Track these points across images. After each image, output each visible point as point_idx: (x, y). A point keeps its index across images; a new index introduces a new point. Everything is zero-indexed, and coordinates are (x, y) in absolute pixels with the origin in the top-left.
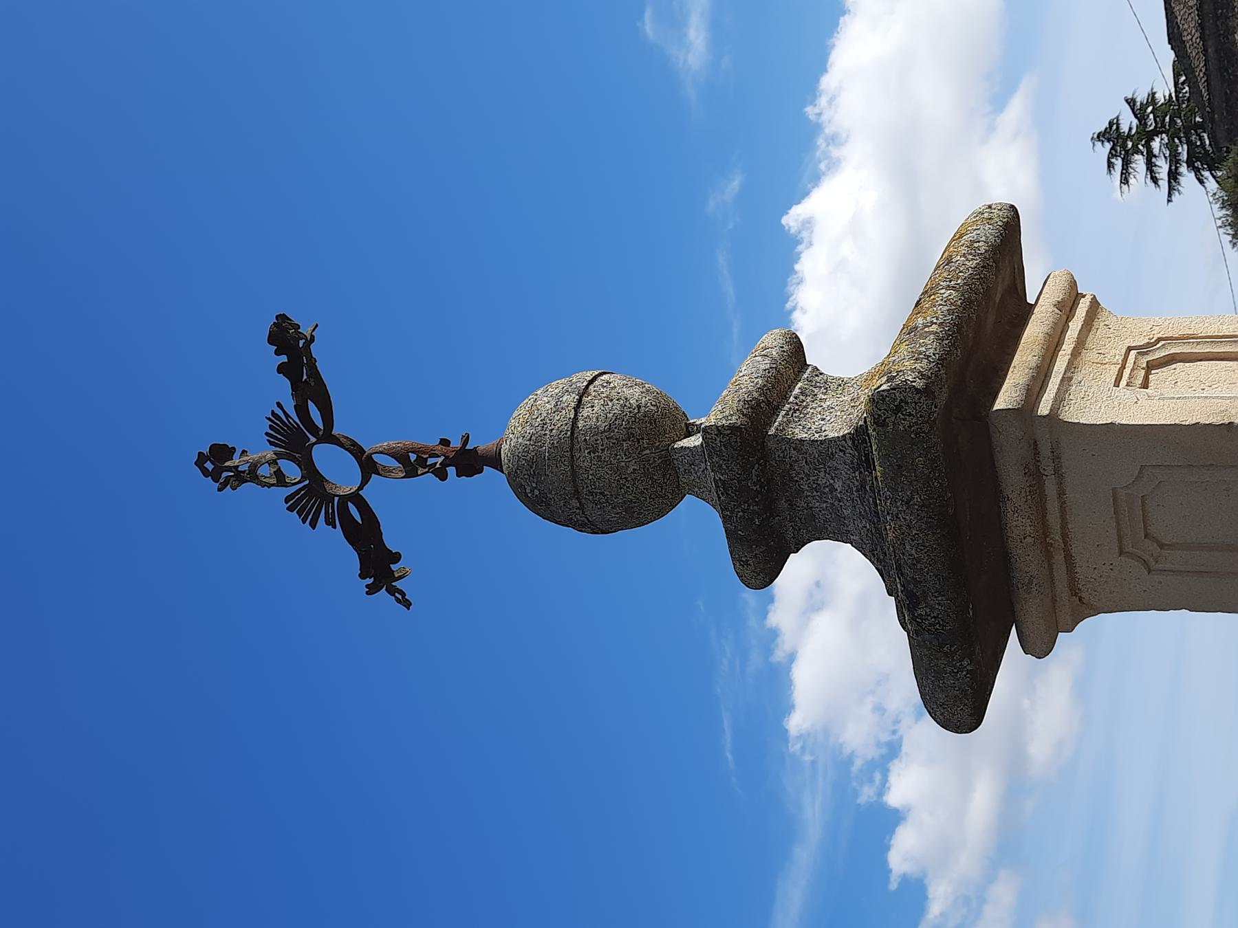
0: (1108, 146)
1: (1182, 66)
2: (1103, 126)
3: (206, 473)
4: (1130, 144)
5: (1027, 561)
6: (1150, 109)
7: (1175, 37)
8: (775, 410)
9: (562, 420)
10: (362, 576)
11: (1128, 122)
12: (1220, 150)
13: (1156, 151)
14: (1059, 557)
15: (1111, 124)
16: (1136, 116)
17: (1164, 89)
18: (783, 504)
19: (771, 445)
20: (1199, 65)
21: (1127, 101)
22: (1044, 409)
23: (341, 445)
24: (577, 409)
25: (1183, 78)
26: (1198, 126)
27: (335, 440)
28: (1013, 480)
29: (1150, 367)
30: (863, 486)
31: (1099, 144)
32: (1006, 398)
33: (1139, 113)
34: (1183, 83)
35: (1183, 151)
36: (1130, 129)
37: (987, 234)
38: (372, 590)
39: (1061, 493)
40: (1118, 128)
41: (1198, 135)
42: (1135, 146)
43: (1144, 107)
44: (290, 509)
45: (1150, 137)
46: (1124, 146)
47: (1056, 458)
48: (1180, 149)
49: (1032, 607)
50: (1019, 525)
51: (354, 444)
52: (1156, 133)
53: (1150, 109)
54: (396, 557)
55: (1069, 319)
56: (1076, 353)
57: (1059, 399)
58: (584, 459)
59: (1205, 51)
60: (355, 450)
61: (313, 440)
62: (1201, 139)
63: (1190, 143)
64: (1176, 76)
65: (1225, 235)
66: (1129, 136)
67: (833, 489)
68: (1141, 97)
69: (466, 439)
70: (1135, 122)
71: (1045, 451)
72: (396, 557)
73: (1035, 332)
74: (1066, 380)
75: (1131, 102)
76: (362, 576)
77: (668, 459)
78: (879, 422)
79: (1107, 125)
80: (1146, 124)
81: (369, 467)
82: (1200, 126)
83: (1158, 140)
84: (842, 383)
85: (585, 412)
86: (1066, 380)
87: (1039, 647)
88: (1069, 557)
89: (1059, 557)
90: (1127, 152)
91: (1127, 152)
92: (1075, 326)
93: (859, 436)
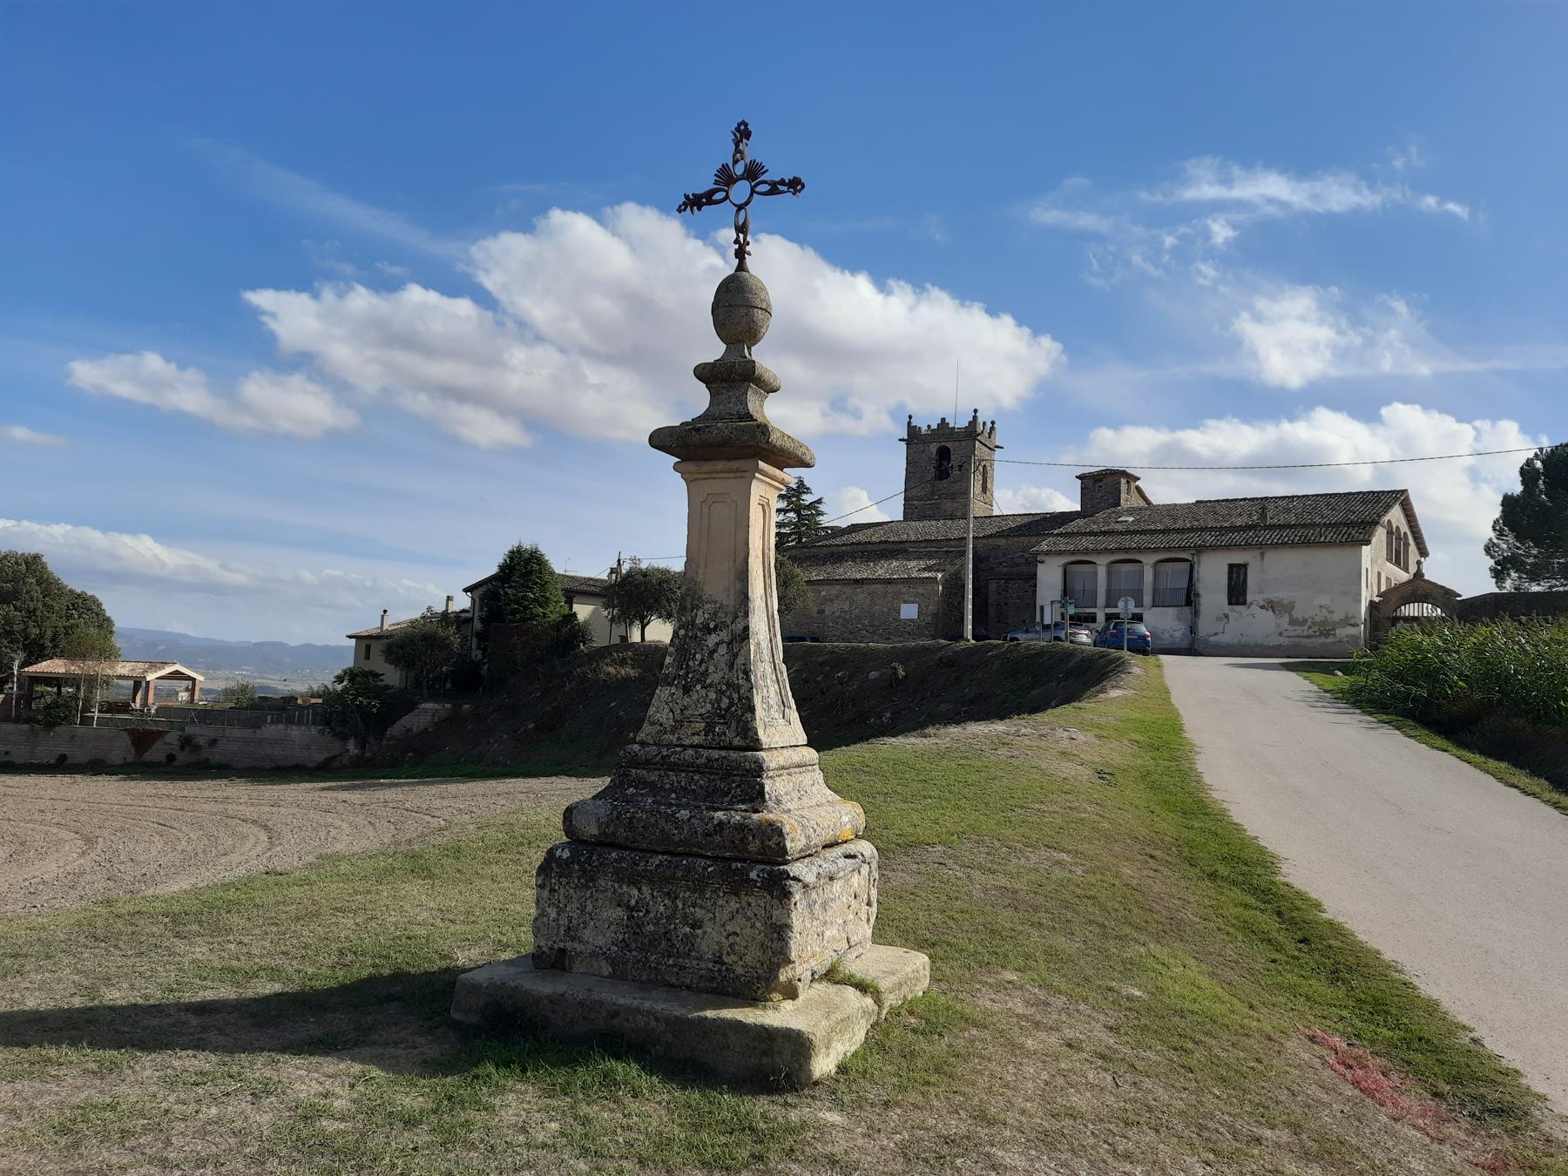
0: (795, 486)
1: (837, 532)
2: (807, 484)
3: (739, 125)
4: (794, 499)
5: (707, 466)
6: (814, 512)
7: (855, 528)
8: (757, 385)
9: (758, 303)
10: (693, 195)
11: (808, 499)
12: (784, 551)
13: (788, 515)
14: (708, 476)
15: (808, 489)
16: (811, 504)
17: (825, 521)
18: (724, 385)
19: (747, 383)
20: (838, 541)
21: (821, 499)
22: (757, 475)
23: (749, 197)
24: (761, 308)
25: (830, 532)
26: (800, 540)
27: (751, 195)
28: (735, 464)
29: (763, 505)
30: (731, 415)
31: (796, 481)
32: (762, 464)
33: (812, 506)
34: (827, 532)
35: (786, 530)
36: (803, 500)
37: (807, 459)
38: (687, 197)
39: (729, 478)
40: (805, 493)
41: (794, 540)
42: (792, 502)
43: (815, 508)
44: (723, 165)
45: (797, 512)
46: (793, 496)
47: (741, 477)
48: (787, 529)
49: (690, 466)
50: (720, 465)
51: (749, 203)
52: (799, 515)
53: (814, 512)
54: (699, 209)
55: (779, 483)
56: (769, 484)
57: (759, 479)
58: (743, 311)
59: (844, 545)
60: (747, 203)
61: (753, 184)
62: (792, 541)
63: (790, 534)
64: (832, 528)
65: (1001, 445)
66: (799, 499)
67: (730, 403)
68: (822, 508)
69: (749, 254)
70: (807, 503)
71: (743, 474)
72: (699, 209)
73: (777, 472)
74: (763, 481)
75: (819, 501)
76: (693, 195)
77: (741, 342)
78: (759, 426)
79: (808, 486)
80: (805, 509)
81: (740, 207)
82: (800, 541)
83: (795, 516)
84: (762, 406)
85: (760, 311)
86: (763, 481)
87: (676, 467)
88: (707, 479)
89: (708, 476)
90: (790, 498)
91: (790, 498)
92: (776, 484)
93: (750, 417)
